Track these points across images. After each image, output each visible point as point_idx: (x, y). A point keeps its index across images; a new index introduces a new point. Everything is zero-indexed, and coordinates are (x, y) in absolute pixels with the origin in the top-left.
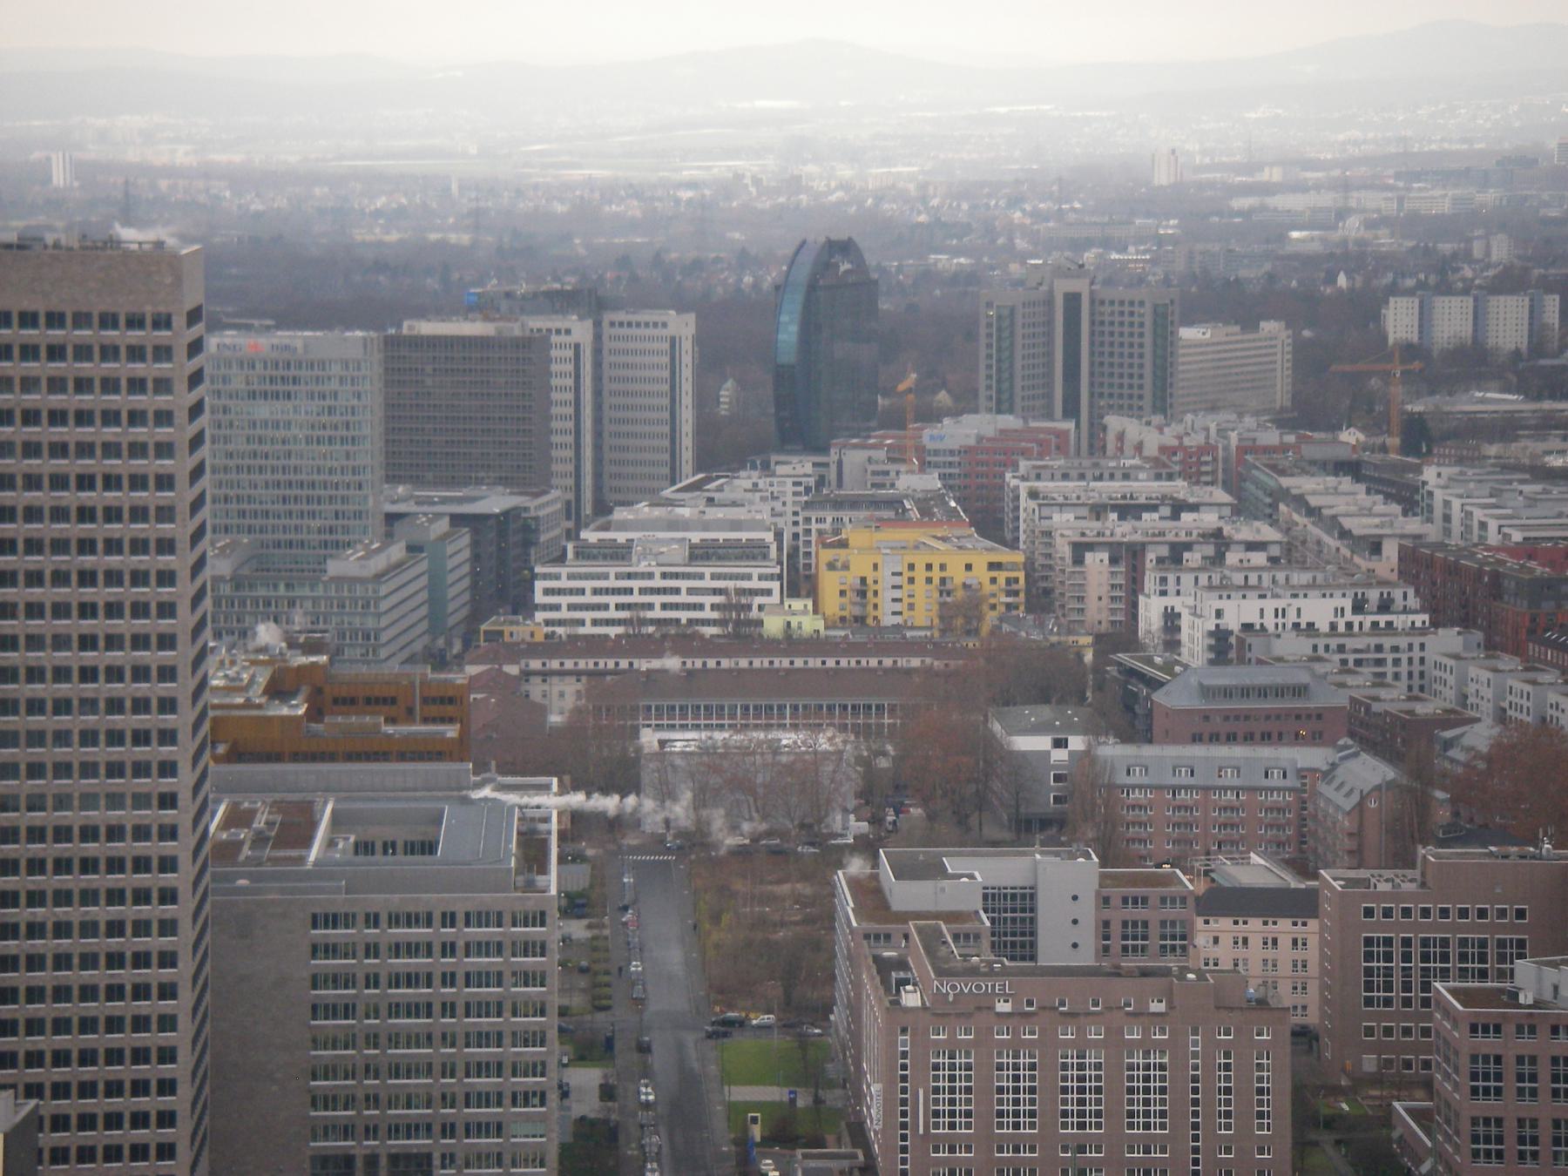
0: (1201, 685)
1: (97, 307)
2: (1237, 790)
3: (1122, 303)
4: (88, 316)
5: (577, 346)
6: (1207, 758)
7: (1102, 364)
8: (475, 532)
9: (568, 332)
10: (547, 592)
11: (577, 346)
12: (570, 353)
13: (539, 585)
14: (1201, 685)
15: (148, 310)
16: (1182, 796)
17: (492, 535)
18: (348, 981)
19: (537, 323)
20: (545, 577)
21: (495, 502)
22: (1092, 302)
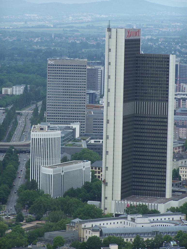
0: (181, 110)
1: (80, 65)
2: (184, 120)
3: (184, 66)
4: (58, 65)
5: (102, 70)
6: (181, 117)
7: (181, 77)
8: (89, 95)
9: (100, 68)
10: (101, 102)
11: (102, 70)
12: (101, 71)
13: (100, 101)
14: (181, 110)
15: (67, 65)
16: (178, 121)
17: (91, 96)
18: (97, 125)
19: (96, 67)
20: (101, 100)
21: (92, 92)
22: (180, 66)
